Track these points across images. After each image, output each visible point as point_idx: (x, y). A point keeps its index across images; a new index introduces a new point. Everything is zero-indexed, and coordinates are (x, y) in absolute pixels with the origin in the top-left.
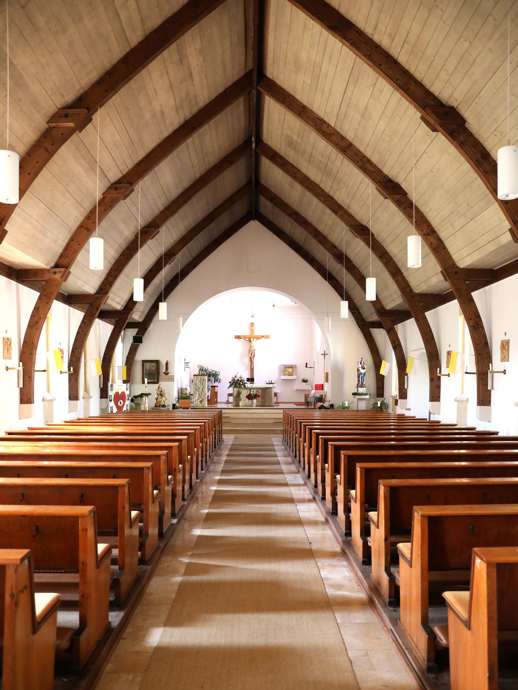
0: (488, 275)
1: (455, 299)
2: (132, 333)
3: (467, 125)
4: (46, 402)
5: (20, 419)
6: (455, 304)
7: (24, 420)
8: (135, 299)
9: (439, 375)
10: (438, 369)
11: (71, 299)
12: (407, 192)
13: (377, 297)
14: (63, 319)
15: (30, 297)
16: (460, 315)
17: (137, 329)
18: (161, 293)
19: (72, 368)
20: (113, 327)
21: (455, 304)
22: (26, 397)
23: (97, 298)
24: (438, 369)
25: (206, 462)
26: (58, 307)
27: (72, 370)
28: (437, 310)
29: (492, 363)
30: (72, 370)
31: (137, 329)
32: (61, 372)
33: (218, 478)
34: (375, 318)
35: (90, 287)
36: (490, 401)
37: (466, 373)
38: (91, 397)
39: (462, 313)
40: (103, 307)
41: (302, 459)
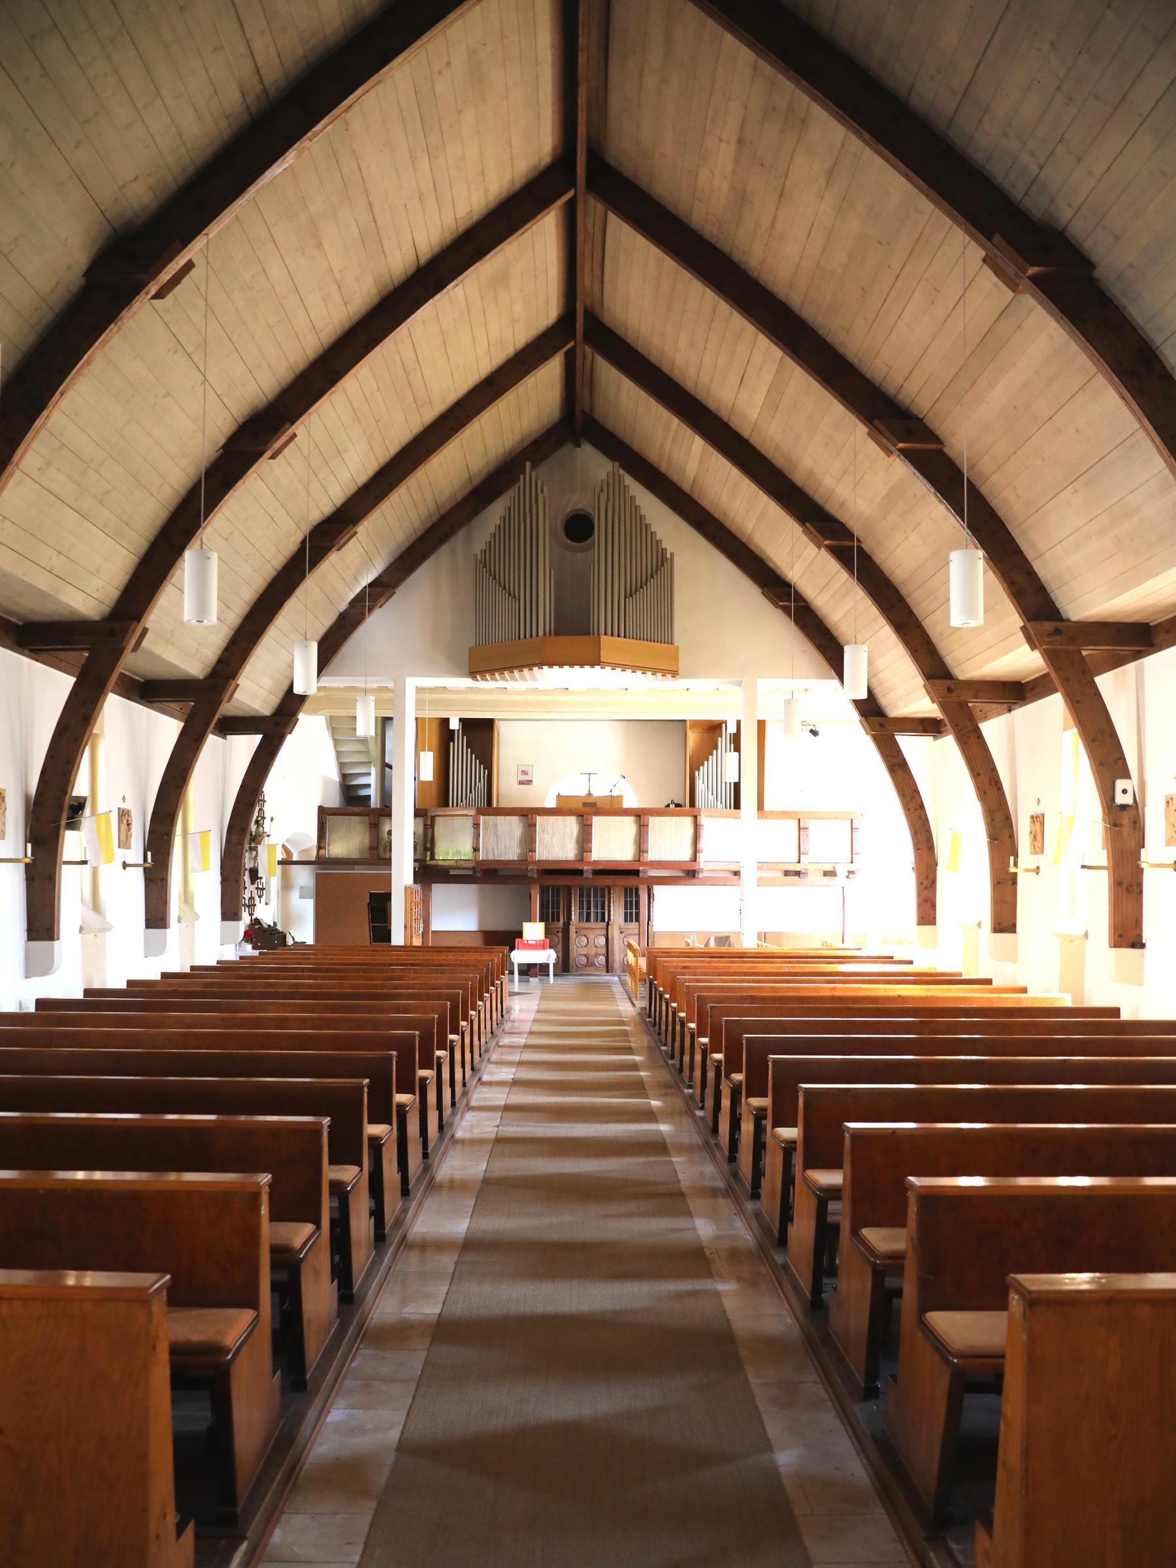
0: (1138, 638)
1: (1056, 691)
2: (246, 745)
3: (1097, 274)
4: (90, 936)
5: (27, 977)
6: (1054, 705)
7: (35, 980)
8: (297, 690)
9: (1012, 870)
10: (1012, 858)
11: (151, 691)
12: (1094, 259)
13: (870, 692)
14: (130, 744)
15: (53, 687)
16: (1065, 729)
17: (259, 737)
18: (199, 481)
19: (149, 854)
20: (182, 724)
21: (1054, 705)
22: (41, 923)
23: (111, 633)
24: (1012, 858)
25: (464, 1085)
26: (115, 711)
27: (149, 860)
28: (1142, 664)
29: (1016, 857)
30: (149, 860)
31: (259, 737)
32: (125, 865)
33: (459, 1226)
34: (924, 706)
35: (88, 594)
36: (1014, 925)
37: (1083, 867)
38: (108, 928)
39: (1071, 721)
40: (228, 708)
41: (663, 1028)
